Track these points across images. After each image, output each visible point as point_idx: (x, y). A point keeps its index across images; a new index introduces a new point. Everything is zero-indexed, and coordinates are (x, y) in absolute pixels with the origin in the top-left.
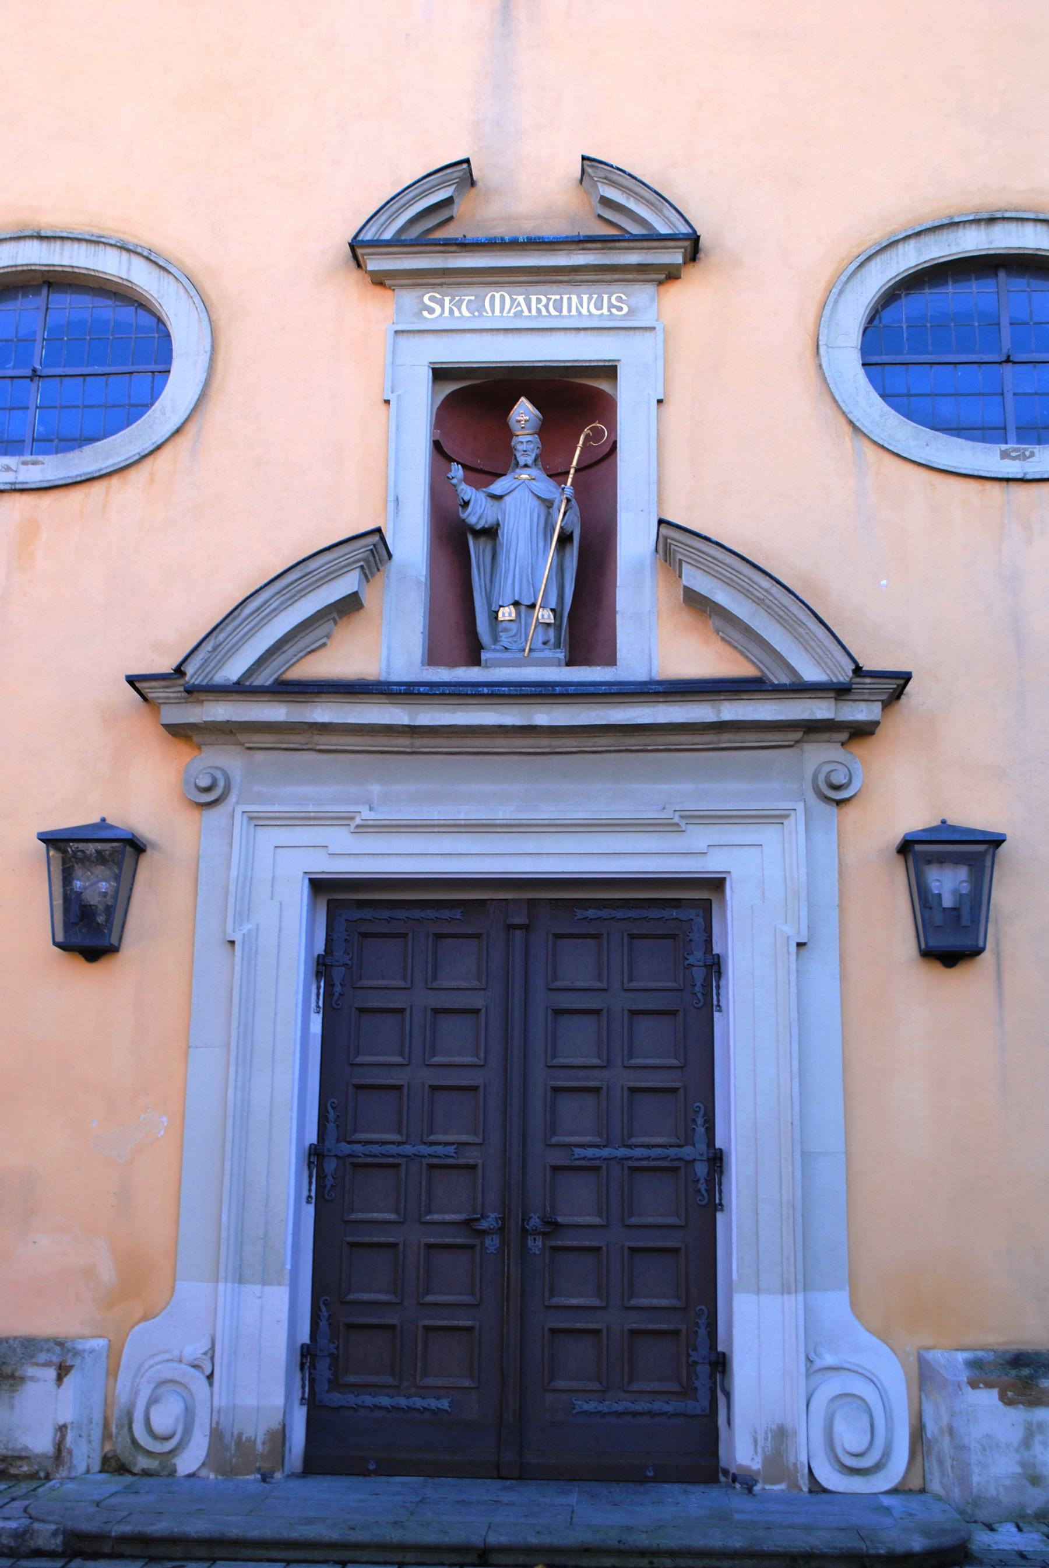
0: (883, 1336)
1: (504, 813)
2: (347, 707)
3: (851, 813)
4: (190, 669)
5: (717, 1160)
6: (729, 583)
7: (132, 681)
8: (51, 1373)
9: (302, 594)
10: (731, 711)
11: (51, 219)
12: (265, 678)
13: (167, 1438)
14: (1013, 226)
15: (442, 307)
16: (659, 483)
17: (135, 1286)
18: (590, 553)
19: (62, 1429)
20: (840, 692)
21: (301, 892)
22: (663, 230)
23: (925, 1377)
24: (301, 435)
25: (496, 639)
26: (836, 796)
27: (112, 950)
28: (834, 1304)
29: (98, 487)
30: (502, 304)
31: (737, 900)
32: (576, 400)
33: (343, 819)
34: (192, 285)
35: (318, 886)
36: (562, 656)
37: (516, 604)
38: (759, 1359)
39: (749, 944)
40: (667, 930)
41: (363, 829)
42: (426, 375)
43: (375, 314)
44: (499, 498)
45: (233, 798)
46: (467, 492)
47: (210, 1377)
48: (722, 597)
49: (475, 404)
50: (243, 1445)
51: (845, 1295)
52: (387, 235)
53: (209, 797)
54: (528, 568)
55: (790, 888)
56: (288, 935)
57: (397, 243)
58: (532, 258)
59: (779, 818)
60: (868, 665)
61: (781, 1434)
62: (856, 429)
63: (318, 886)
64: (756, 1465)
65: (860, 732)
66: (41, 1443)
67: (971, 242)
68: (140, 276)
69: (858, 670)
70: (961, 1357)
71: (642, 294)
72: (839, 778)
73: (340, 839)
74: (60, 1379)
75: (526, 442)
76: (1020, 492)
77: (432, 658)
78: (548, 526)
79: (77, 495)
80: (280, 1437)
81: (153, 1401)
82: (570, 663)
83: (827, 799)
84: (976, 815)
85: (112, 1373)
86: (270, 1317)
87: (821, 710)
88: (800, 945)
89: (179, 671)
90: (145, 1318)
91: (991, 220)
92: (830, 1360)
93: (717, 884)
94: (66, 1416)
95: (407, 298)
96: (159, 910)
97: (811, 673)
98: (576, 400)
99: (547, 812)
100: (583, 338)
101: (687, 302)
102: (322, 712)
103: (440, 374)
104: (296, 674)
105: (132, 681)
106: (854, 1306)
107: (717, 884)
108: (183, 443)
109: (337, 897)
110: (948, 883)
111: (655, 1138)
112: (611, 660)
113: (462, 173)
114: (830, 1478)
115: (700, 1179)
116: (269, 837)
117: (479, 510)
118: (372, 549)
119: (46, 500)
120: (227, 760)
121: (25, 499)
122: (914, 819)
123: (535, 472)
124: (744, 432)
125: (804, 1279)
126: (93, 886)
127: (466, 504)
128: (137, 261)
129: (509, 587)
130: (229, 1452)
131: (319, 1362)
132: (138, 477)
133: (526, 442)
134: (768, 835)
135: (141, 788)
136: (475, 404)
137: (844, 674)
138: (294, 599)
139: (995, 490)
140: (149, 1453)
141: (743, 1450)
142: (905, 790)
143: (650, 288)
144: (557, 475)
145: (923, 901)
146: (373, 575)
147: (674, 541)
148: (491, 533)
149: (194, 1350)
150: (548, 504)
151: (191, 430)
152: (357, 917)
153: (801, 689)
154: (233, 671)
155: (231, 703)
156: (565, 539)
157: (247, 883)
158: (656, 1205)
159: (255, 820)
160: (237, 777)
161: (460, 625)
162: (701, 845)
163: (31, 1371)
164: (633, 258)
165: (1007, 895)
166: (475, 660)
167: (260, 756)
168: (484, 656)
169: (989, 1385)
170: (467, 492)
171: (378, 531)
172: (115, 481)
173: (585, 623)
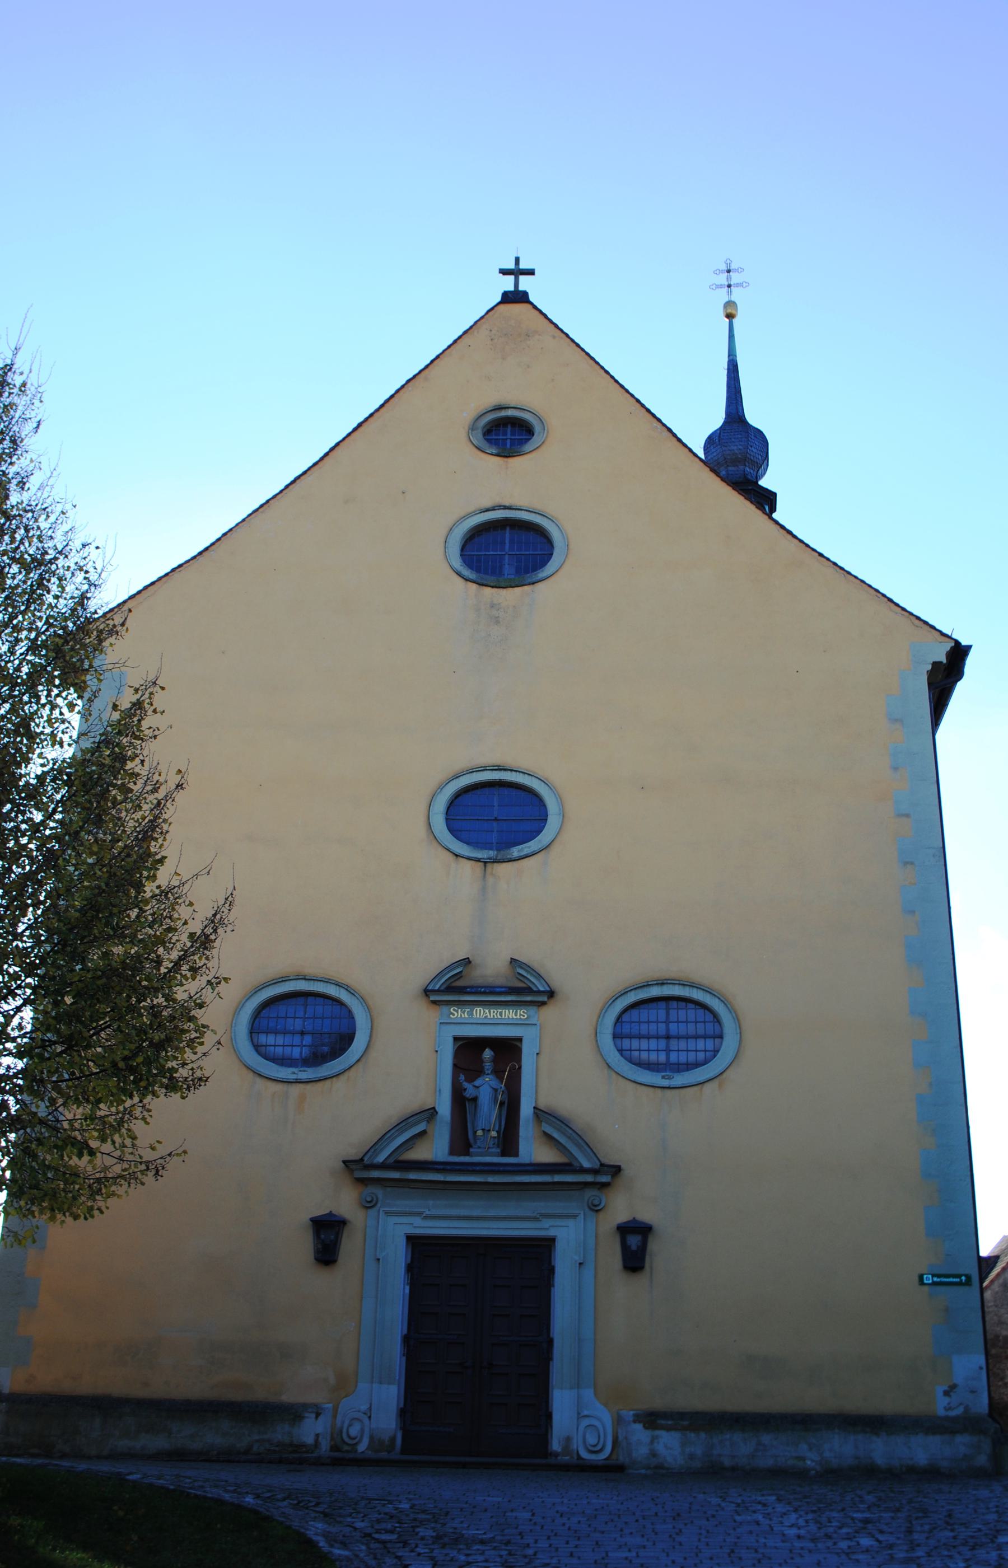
0: (605, 1405)
1: (476, 1213)
3: (601, 1215)
4: (366, 1159)
5: (550, 1342)
6: (558, 1130)
7: (344, 1162)
8: (313, 1415)
9: (406, 1130)
10: (558, 1178)
11: (309, 971)
12: (391, 1160)
13: (355, 1438)
14: (671, 986)
15: (458, 1014)
16: (537, 1086)
17: (343, 1385)
19: (317, 1435)
21: (402, 1242)
22: (541, 989)
23: (619, 1421)
24: (404, 1067)
25: (476, 1142)
26: (596, 1209)
28: (588, 1393)
29: (328, 1082)
30: (480, 1013)
31: (559, 1246)
32: (508, 1050)
33: (420, 1214)
34: (363, 1000)
36: (499, 1150)
37: (483, 1130)
38: (730, 316)
39: (564, 1262)
41: (426, 1218)
42: (451, 1040)
43: (431, 1016)
44: (478, 1087)
45: (379, 1205)
46: (466, 1085)
47: (370, 1417)
49: (469, 1053)
51: (592, 1390)
52: (437, 988)
53: (369, 1205)
54: (488, 1114)
55: (577, 1240)
56: (398, 1256)
58: (490, 994)
59: (575, 1216)
60: (606, 1161)
61: (568, 1439)
62: (609, 1067)
64: (559, 1450)
66: (310, 1440)
67: (655, 992)
69: (602, 1165)
70: (632, 1413)
71: (533, 1010)
72: (596, 1202)
73: (417, 1221)
74: (317, 1418)
75: (488, 1066)
76: (668, 1092)
77: (452, 1152)
78: (496, 1099)
79: (320, 1084)
80: (393, 1440)
81: (350, 1425)
82: (503, 1154)
83: (593, 1210)
84: (646, 1216)
85: (335, 1417)
86: (389, 1397)
87: (589, 1178)
88: (580, 1264)
89: (362, 1160)
90: (346, 1396)
91: (663, 984)
92: (586, 1413)
93: (552, 1240)
94: (319, 1430)
95: (444, 1009)
96: (350, 1246)
97: (586, 1164)
98: (508, 1050)
99: (492, 1213)
100: (509, 1027)
101: (549, 1014)
102: (412, 1176)
103: (456, 1039)
105: (344, 1162)
106: (595, 1394)
107: (552, 1240)
108: (360, 1065)
109: (413, 1241)
110: (634, 1241)
112: (516, 1155)
113: (467, 962)
114: (585, 1455)
115: (543, 1348)
117: (470, 1091)
118: (431, 1113)
119: (309, 1086)
120: (379, 1192)
121: (301, 1085)
122: (622, 1216)
123: (491, 1076)
124: (567, 1069)
125: (577, 1385)
127: (465, 1090)
128: (342, 990)
129: (481, 1123)
130: (375, 1443)
132: (343, 1078)
133: (488, 1066)
134: (571, 1223)
135: (345, 1202)
136: (469, 1053)
137: (597, 1166)
138: (402, 1132)
139: (659, 1091)
140: (348, 1444)
141: (556, 1446)
142: (620, 1208)
143: (535, 1008)
144: (501, 1079)
145: (625, 1247)
147: (539, 1113)
148: (475, 1099)
149: (364, 1407)
150: (496, 1090)
151: (363, 1060)
153: (583, 1171)
154: (381, 1158)
155: (379, 1171)
156: (502, 1104)
157: (385, 1236)
160: (380, 1197)
161: (462, 1139)
162: (547, 1226)
163: (307, 1415)
164: (529, 998)
165: (653, 1246)
166: (467, 1153)
167: (389, 1189)
168: (471, 1150)
169: (640, 1422)
170: (466, 1085)
171: (434, 1108)
172: (334, 1079)
173: (508, 1141)
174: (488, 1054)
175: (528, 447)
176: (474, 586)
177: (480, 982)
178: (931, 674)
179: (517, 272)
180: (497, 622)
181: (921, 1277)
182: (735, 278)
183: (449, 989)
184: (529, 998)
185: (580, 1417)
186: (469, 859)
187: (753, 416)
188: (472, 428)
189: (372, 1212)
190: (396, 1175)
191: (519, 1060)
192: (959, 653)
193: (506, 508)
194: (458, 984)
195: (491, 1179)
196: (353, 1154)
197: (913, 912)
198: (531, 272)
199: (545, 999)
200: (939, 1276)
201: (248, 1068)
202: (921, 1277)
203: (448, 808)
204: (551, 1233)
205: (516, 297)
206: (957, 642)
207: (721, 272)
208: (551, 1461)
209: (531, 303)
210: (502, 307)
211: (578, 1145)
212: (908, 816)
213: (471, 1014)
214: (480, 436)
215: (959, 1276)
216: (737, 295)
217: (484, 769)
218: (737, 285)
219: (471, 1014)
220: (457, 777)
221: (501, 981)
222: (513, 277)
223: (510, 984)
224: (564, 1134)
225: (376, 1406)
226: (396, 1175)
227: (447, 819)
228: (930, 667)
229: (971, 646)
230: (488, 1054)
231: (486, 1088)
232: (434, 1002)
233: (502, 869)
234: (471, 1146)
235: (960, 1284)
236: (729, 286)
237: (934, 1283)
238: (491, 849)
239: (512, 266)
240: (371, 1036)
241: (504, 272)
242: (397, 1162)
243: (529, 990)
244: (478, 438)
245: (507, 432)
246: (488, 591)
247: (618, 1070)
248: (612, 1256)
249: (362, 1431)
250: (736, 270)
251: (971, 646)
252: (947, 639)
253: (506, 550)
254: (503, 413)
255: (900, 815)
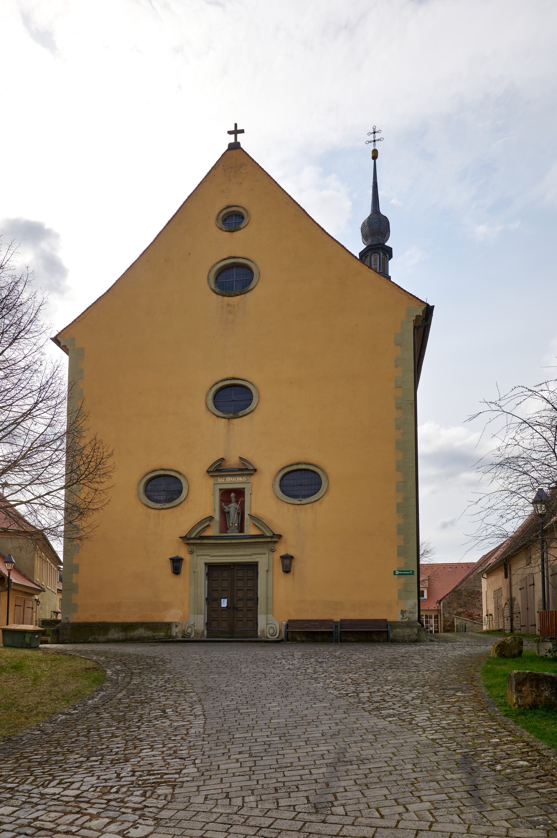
2: (26, 628)
3: (275, 553)
11: (165, 467)
12: (198, 536)
15: (220, 480)
18: (241, 514)
20: (271, 537)
21: (203, 566)
24: (201, 501)
27: (180, 573)
30: (228, 479)
32: (240, 493)
35: (206, 564)
40: (254, 566)
41: (211, 556)
43: (211, 481)
46: (225, 507)
48: (257, 524)
49: (226, 495)
50: (198, 634)
54: (233, 518)
55: (266, 562)
56: (202, 571)
57: (212, 472)
59: (265, 554)
60: (276, 533)
63: (206, 564)
65: (276, 542)
67: (295, 467)
68: (178, 476)
69: (274, 534)
71: (248, 477)
73: (208, 558)
75: (233, 499)
76: (300, 506)
77: (221, 532)
84: (291, 553)
85: (182, 626)
87: (269, 540)
93: (257, 562)
95: (215, 478)
96: (185, 568)
97: (268, 535)
98: (240, 493)
99: (235, 554)
101: (254, 479)
102: (205, 541)
104: (202, 535)
107: (257, 562)
108: (185, 501)
110: (287, 562)
111: (250, 595)
113: (222, 459)
114: (268, 636)
116: (199, 558)
117: (227, 509)
118: (211, 518)
120: (194, 548)
121: (164, 511)
122: (283, 553)
126: (176, 565)
129: (231, 521)
131: (208, 624)
133: (233, 499)
137: (272, 535)
141: (259, 634)
142: (282, 550)
146: (183, 540)
148: (229, 512)
152: (211, 568)
153: (267, 537)
154: (193, 536)
155: (194, 540)
157: (196, 563)
158: (250, 604)
159: (198, 555)
161: (225, 527)
164: (246, 472)
165: (294, 563)
170: (225, 507)
173: (241, 528)
174: (233, 495)
175: (242, 226)
176: (221, 297)
177: (228, 467)
178: (416, 321)
179: (236, 132)
180: (231, 313)
181: (394, 572)
182: (378, 136)
183: (217, 471)
184: (246, 472)
185: (267, 624)
186: (223, 418)
187: (383, 211)
188: (217, 219)
189: (192, 555)
190: (199, 541)
191: (244, 497)
192: (429, 310)
193: (234, 257)
194: (220, 468)
195: (233, 541)
196: (184, 534)
197: (400, 429)
198: (242, 131)
199: (253, 472)
200: (401, 571)
201: (145, 505)
202: (394, 572)
203: (215, 397)
204: (256, 560)
205: (235, 147)
206: (428, 305)
207: (371, 133)
208: (258, 639)
209: (242, 149)
210: (228, 152)
211: (264, 527)
212: (400, 387)
213: (225, 480)
214: (221, 222)
215: (409, 571)
216: (379, 146)
217: (227, 379)
218: (379, 140)
219: (225, 480)
220: (216, 383)
221: (236, 467)
222: (234, 135)
223: (240, 467)
224: (260, 523)
225: (199, 622)
226: (199, 541)
227: (214, 402)
228: (414, 318)
229: (434, 306)
230: (233, 495)
231: (233, 507)
232: (211, 476)
233: (235, 421)
234: (228, 529)
235: (410, 574)
236: (374, 141)
237: (399, 574)
238: (231, 413)
239: (233, 129)
240: (188, 490)
241: (230, 133)
242: (200, 537)
243: (247, 469)
244: (220, 224)
245: (232, 220)
246: (226, 299)
247: (281, 499)
248: (278, 568)
249: (192, 630)
250: (378, 132)
251: (434, 306)
252: (423, 304)
253: (234, 278)
254: (230, 209)
255: (396, 387)
